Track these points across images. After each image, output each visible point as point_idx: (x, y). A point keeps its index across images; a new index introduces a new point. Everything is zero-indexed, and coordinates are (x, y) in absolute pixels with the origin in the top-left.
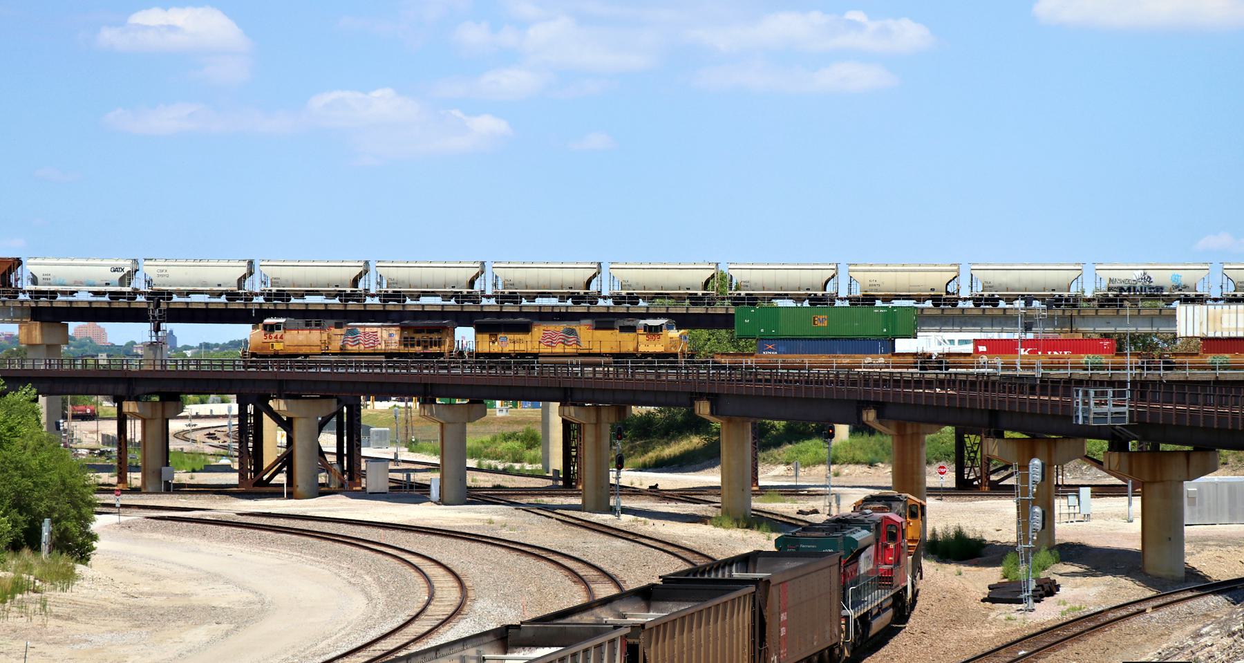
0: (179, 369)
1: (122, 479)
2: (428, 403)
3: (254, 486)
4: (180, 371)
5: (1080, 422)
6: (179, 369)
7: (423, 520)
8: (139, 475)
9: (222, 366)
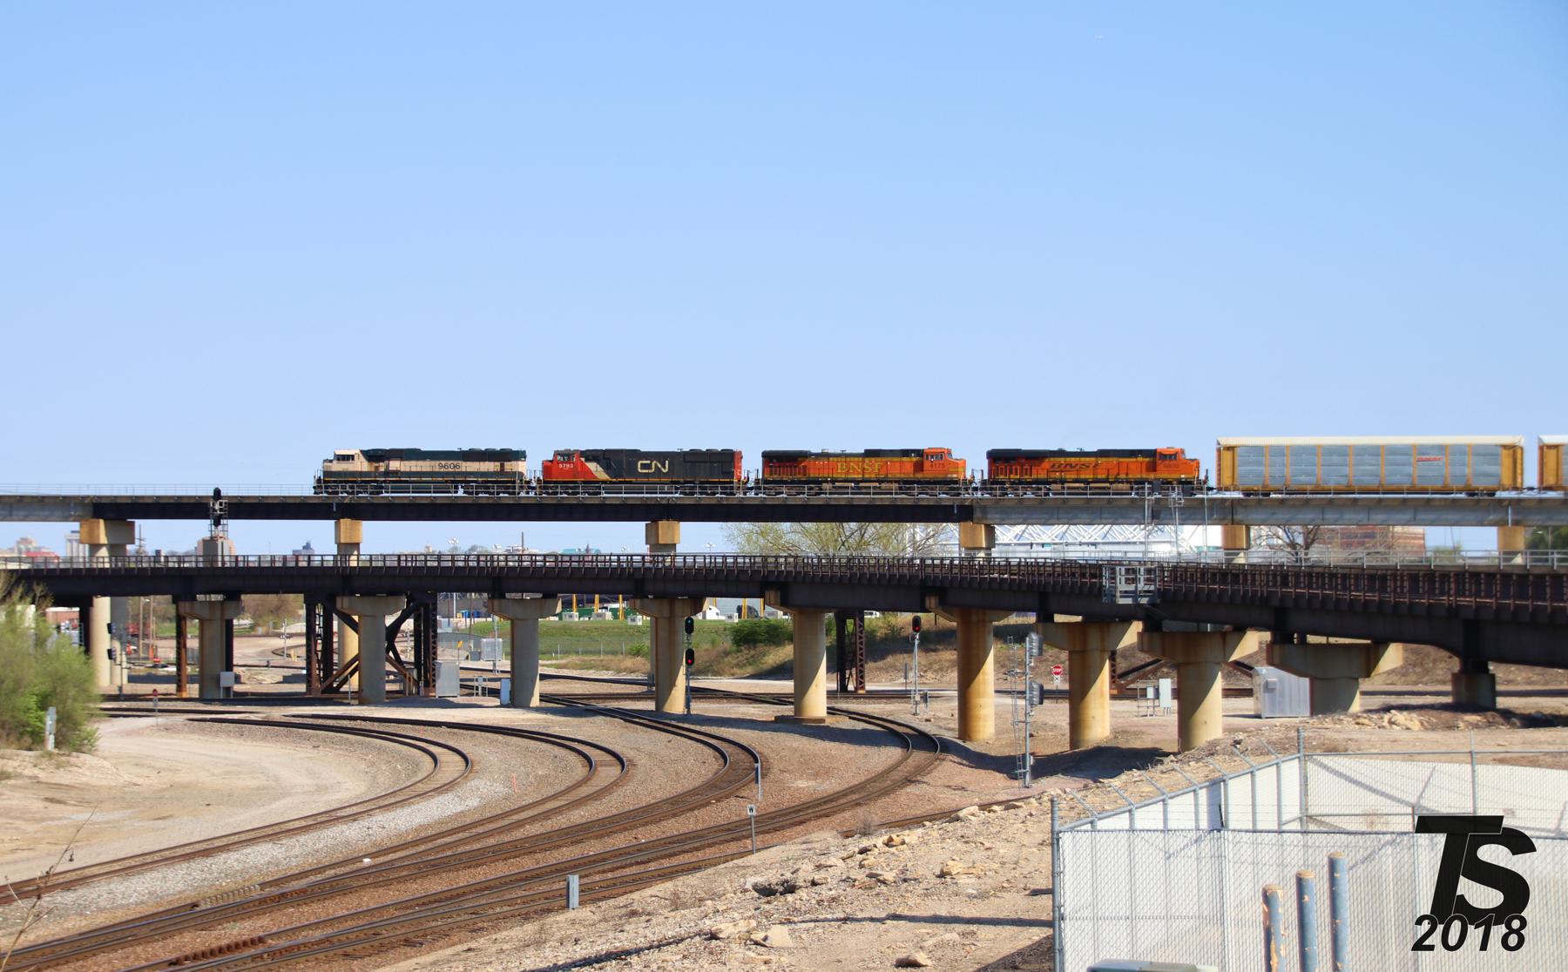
0: (402, 565)
1: (180, 689)
2: (348, 596)
3: (323, 692)
4: (403, 567)
5: (220, 565)
6: (402, 565)
7: (479, 720)
8: (196, 686)
9: (426, 561)
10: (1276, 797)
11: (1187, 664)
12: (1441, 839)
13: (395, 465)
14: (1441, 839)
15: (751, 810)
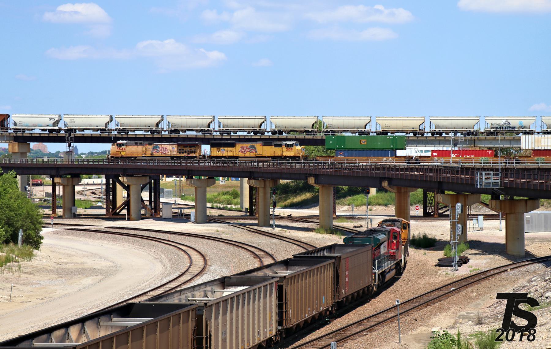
1: (54, 212)
5: (479, 187)
8: (61, 210)
9: (98, 162)
10: (187, 237)
11: (511, 213)
12: (505, 301)
13: (397, 134)
14: (505, 301)
15: (398, 302)
